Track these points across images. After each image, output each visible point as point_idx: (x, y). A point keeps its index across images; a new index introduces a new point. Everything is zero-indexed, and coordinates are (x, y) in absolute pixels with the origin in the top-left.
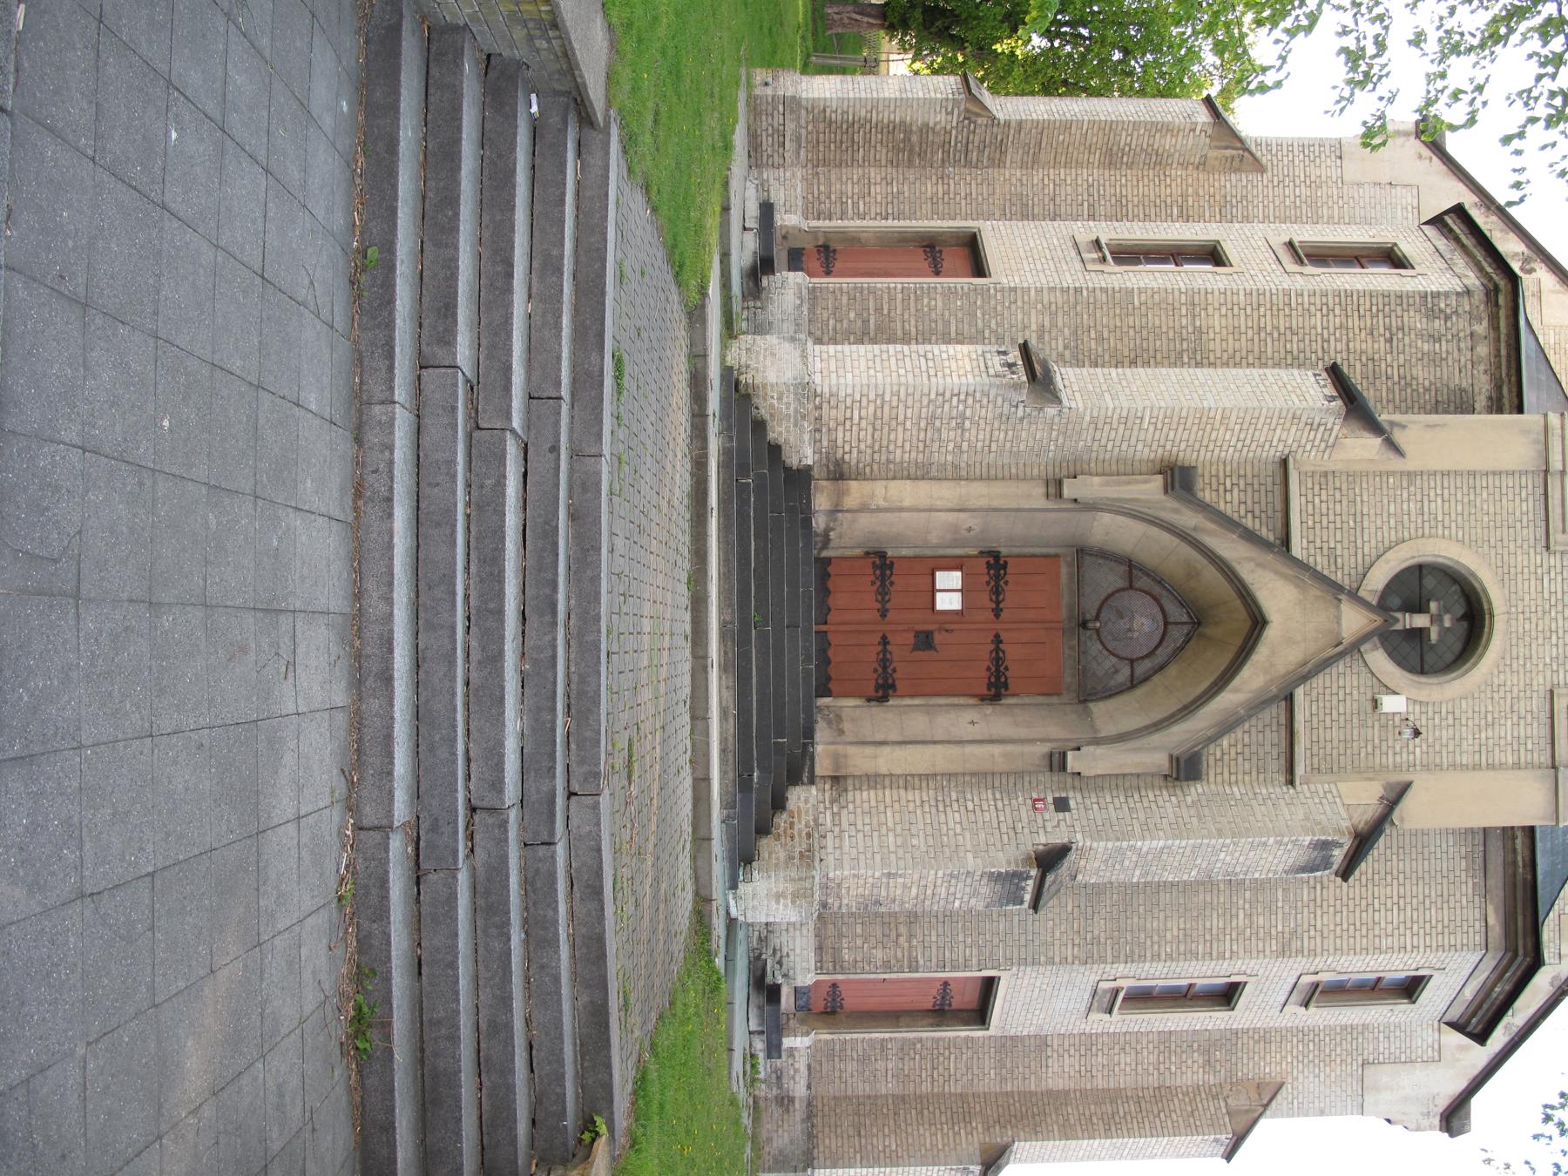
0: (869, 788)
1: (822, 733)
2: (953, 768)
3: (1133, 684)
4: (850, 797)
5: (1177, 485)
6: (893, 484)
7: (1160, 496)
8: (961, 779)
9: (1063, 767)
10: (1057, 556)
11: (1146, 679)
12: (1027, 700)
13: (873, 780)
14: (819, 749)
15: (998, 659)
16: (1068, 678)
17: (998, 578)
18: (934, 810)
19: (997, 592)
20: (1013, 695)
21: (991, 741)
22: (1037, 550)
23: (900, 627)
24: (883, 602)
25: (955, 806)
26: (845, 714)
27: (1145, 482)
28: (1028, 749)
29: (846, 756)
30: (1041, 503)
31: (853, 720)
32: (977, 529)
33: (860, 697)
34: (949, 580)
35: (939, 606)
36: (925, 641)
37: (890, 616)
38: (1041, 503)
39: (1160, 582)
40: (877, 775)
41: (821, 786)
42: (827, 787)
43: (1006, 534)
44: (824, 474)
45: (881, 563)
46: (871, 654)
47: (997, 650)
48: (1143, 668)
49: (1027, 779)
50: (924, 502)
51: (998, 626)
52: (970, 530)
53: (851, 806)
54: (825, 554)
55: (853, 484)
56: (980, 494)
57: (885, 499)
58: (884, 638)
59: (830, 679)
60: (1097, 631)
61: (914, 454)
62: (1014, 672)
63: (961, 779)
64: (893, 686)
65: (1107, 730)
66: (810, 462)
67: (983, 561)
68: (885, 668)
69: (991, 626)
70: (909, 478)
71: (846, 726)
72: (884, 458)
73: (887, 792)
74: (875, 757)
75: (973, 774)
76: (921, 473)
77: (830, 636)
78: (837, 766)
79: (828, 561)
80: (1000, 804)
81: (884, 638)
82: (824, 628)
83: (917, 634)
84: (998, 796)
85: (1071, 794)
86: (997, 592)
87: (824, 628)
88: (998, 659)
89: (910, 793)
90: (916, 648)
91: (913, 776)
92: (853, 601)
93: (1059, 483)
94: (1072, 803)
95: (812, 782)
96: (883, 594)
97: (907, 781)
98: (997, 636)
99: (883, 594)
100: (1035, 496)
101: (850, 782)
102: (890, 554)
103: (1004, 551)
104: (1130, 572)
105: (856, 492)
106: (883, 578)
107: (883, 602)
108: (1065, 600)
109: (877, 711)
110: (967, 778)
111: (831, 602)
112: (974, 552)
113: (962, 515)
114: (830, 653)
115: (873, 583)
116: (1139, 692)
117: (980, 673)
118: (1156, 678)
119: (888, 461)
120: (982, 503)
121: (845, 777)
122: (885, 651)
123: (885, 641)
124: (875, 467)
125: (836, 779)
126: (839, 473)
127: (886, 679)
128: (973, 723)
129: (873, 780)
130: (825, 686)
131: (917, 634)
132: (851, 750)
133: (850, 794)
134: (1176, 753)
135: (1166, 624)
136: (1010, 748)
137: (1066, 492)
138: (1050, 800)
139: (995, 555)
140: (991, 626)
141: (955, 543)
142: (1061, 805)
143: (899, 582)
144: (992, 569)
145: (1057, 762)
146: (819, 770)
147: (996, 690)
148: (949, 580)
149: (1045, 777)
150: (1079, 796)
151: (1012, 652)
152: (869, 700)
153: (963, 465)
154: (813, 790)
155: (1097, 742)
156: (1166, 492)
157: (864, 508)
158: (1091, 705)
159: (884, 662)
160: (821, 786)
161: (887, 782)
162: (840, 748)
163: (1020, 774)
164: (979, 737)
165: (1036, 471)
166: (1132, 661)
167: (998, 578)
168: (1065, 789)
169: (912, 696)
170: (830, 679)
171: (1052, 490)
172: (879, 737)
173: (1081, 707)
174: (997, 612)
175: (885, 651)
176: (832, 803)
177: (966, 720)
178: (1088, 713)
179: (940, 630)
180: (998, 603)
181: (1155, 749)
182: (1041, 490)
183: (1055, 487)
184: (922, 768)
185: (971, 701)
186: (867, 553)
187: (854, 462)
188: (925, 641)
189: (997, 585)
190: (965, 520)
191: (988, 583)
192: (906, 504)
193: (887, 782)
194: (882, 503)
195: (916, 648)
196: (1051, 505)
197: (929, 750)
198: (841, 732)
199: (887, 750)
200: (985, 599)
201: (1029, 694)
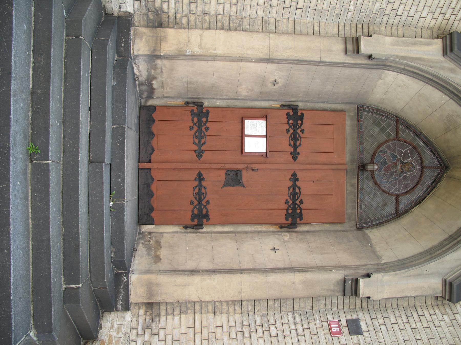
0: (181, 312)
1: (140, 262)
2: (258, 295)
3: (398, 214)
4: (162, 324)
5: (455, 47)
6: (207, 33)
7: (440, 57)
8: (264, 304)
9: (355, 292)
10: (342, 111)
11: (406, 211)
12: (317, 228)
13: (184, 306)
14: (134, 278)
15: (295, 194)
16: (350, 210)
17: (296, 127)
18: (240, 336)
19: (295, 138)
20: (306, 224)
21: (292, 270)
22: (327, 106)
23: (214, 166)
24: (200, 144)
25: (260, 330)
26: (165, 240)
27: (428, 44)
28: (324, 276)
29: (159, 285)
30: (340, 58)
31: (171, 246)
32: (281, 82)
33: (178, 224)
34: (255, 127)
35: (247, 149)
36: (234, 178)
37: (205, 156)
38: (340, 58)
39: (418, 134)
40: (188, 302)
41: (135, 311)
42: (142, 312)
43: (306, 86)
44: (144, 23)
45: (198, 112)
46: (189, 189)
47: (294, 186)
48: (404, 202)
49: (322, 302)
50: (236, 51)
51: (295, 167)
52: (275, 83)
53: (162, 333)
54: (151, 103)
55: (171, 32)
56: (285, 46)
57: (200, 46)
58: (200, 175)
59: (152, 209)
60: (372, 172)
61: (227, 6)
62: (307, 204)
63: (264, 304)
64: (207, 216)
65: (388, 256)
66: (130, 9)
67: (284, 112)
68: (200, 201)
69: (288, 167)
70: (222, 28)
71: (164, 253)
72: (200, 9)
73: (197, 317)
74: (186, 285)
75: (276, 300)
76: (235, 25)
77: (153, 173)
78: (150, 294)
79: (153, 108)
80: (299, 327)
81: (200, 175)
82: (147, 165)
83: (228, 172)
84: (298, 319)
85: (361, 316)
86: (295, 138)
87: (147, 165)
88: (295, 194)
89: (218, 317)
90: (227, 184)
91: (221, 302)
92: (175, 142)
93: (357, 40)
94: (363, 325)
95: (126, 308)
96: (200, 137)
97: (215, 307)
98: (294, 175)
99: (200, 137)
100: (335, 52)
101: (163, 307)
102: (206, 104)
103: (301, 105)
104: (397, 126)
105: (173, 40)
106: (199, 124)
107: (200, 144)
108: (348, 147)
109: (193, 238)
110: (270, 303)
111: (155, 143)
112: (276, 105)
113: (270, 67)
114: (153, 187)
115: (191, 128)
116: (406, 220)
117: (280, 205)
118: (416, 210)
119: (205, 13)
120: (289, 54)
121: (158, 304)
122: (200, 186)
123: (200, 178)
124: (192, 18)
125: (149, 306)
126: (158, 21)
127: (200, 210)
128: (274, 249)
129: (184, 306)
130: (149, 215)
131: (228, 172)
132: (164, 279)
133: (163, 319)
134: (449, 279)
135: (423, 167)
136: (309, 276)
137: (365, 48)
138: (344, 322)
139: (295, 108)
140: (288, 167)
141: (262, 96)
142: (354, 328)
143: (213, 127)
144: (292, 119)
145: (350, 288)
146: (133, 298)
147: (292, 219)
148: (255, 127)
149: (339, 301)
150: (367, 316)
151: (306, 189)
152: (186, 227)
153: (272, 20)
154: (128, 316)
155: (384, 268)
156: (445, 53)
157: (179, 56)
158: (368, 232)
159: (200, 195)
160: (135, 311)
161: (197, 307)
162: (153, 277)
163: (317, 299)
164: (281, 265)
165: (335, 30)
166: (397, 197)
167: (296, 127)
168: (354, 310)
169: (223, 224)
170: (152, 209)
171: (350, 47)
172: (191, 265)
173: (359, 233)
174: (295, 155)
175: (200, 186)
176: (144, 329)
177: (268, 247)
178: (368, 240)
179: (247, 169)
180: (295, 147)
181: (432, 274)
182: (341, 46)
183: (353, 44)
184: (230, 295)
185: (272, 229)
186: (187, 103)
187: (172, 11)
188: (234, 178)
189: (295, 133)
190: (273, 72)
191: (288, 131)
192: (220, 51)
193: (197, 307)
194: (197, 50)
195: (227, 184)
196: (349, 60)
197: (237, 278)
198: (157, 259)
199: (197, 279)
200: (285, 144)
201: (317, 223)
